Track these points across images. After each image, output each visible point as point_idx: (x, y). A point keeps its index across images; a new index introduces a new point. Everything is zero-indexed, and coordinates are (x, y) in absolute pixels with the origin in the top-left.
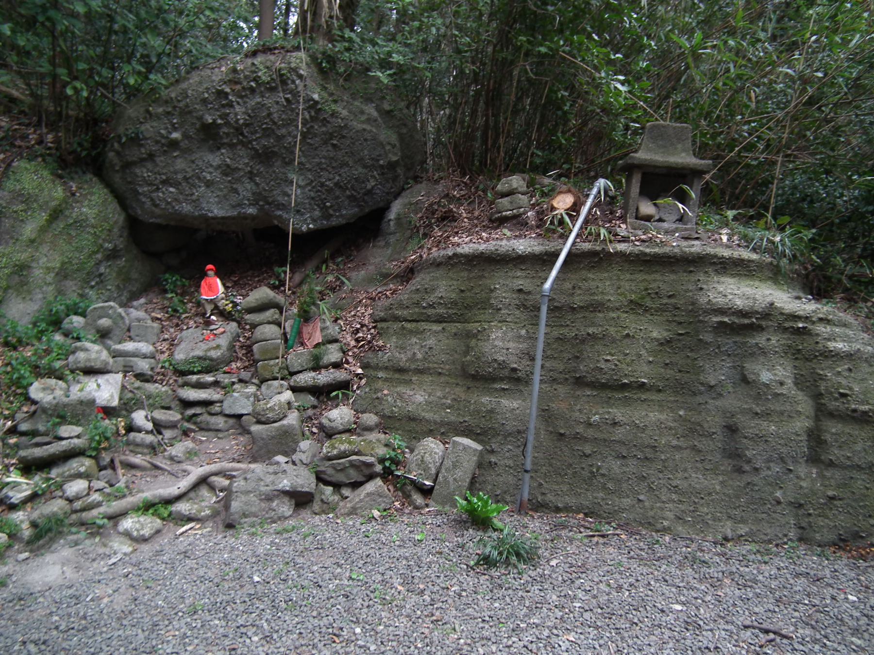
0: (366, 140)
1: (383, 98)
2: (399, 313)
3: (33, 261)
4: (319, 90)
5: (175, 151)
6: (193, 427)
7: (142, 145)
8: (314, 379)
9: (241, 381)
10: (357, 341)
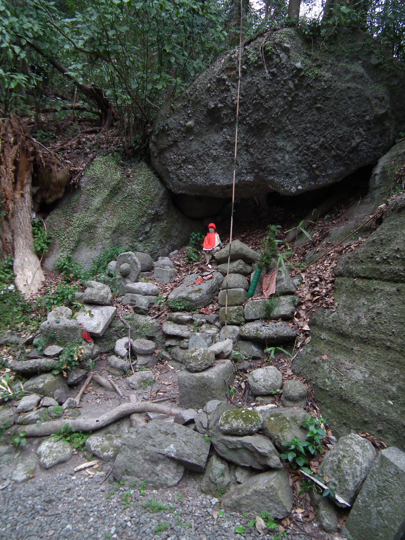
0: (350, 98)
1: (372, 52)
2: (353, 268)
3: (98, 223)
4: (303, 59)
5: (191, 136)
6: (168, 356)
7: (169, 135)
8: (257, 330)
9: (208, 322)
10: (313, 294)
